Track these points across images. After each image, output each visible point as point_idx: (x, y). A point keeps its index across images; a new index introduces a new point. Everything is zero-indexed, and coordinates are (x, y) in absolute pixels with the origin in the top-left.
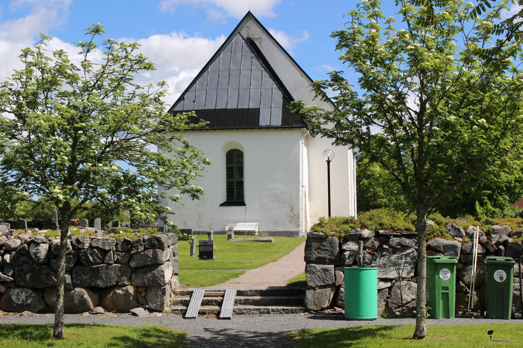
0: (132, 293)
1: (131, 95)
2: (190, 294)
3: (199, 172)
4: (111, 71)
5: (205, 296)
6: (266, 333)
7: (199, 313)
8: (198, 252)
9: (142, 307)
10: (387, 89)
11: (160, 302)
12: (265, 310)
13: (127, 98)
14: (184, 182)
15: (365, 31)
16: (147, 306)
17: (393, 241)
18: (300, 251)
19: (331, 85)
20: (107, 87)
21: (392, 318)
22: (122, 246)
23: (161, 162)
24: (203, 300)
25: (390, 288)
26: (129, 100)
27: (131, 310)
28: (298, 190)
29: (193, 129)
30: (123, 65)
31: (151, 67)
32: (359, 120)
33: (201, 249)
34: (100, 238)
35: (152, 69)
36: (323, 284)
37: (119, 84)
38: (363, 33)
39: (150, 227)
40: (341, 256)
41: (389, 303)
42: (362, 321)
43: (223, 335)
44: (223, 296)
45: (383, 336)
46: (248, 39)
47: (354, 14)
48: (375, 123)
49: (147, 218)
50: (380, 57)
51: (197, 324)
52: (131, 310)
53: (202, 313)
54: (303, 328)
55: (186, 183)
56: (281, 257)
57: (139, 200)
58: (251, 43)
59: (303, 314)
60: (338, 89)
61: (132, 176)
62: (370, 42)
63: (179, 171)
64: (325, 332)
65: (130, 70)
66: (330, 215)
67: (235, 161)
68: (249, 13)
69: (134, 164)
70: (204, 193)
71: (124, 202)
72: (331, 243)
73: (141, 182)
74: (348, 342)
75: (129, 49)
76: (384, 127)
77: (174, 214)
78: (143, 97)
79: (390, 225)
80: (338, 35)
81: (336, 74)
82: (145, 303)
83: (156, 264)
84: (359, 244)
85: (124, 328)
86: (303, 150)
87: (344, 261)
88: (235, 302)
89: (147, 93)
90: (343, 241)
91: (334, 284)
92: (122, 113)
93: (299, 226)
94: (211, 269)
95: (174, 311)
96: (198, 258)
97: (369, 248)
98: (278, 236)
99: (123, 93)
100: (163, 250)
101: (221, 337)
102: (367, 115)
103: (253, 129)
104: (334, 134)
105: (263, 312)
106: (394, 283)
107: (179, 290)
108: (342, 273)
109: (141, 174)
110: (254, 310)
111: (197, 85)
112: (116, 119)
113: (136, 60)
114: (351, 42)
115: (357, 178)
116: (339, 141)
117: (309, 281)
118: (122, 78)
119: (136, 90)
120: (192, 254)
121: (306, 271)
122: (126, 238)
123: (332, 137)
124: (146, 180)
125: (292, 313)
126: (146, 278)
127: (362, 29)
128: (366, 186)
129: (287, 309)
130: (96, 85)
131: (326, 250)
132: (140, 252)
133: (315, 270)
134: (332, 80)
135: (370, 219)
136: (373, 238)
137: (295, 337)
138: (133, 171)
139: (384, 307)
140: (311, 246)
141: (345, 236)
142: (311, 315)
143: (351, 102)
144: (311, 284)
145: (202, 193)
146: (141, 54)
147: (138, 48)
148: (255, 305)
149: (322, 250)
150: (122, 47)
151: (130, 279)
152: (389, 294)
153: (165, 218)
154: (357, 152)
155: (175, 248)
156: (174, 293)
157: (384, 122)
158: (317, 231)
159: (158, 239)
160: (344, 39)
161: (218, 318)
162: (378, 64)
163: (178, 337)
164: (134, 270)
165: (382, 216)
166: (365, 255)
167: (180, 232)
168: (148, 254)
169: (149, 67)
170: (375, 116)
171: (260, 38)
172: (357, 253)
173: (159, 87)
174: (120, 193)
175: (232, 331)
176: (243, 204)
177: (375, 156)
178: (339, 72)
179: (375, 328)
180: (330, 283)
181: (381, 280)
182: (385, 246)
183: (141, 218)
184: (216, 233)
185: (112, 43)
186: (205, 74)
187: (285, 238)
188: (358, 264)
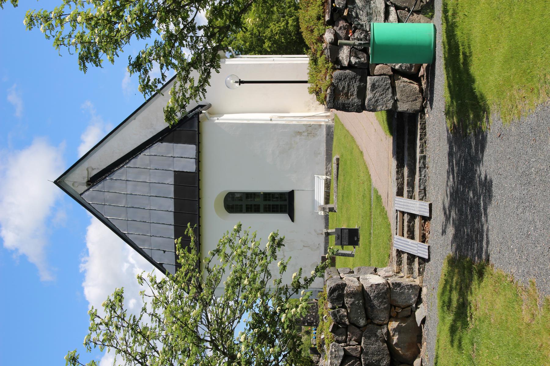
0: (397, 323)
1: (154, 319)
2: (400, 253)
3: (250, 237)
4: (125, 343)
5: (403, 235)
6: (449, 159)
7: (424, 242)
8: (349, 246)
9: (415, 312)
10: (151, 5)
11: (409, 289)
12: (422, 162)
13: (158, 323)
14: (262, 256)
15: (80, 29)
16: (414, 305)
17: (339, 3)
18: (349, 118)
19: (146, 71)
20: (144, 347)
21: (433, 6)
22: (339, 335)
23: (236, 283)
24: (407, 237)
25: (397, 8)
26: (160, 321)
27: (419, 325)
28: (276, 125)
29: (199, 244)
30: (117, 327)
31: (120, 293)
32: (189, 39)
33: (345, 243)
34: (329, 361)
35: (122, 293)
36: (390, 90)
37: (140, 333)
38: (81, 31)
39: (317, 303)
40: (356, 67)
41: (415, 9)
42: (437, 42)
43: (450, 212)
44: (403, 213)
45: (454, 14)
46: (89, 184)
47: (60, 42)
48: (193, 19)
49: (306, 300)
50: (112, 11)
51: (436, 243)
52: (419, 325)
53: (423, 239)
54: (443, 114)
55: (264, 253)
56: (358, 147)
57: (283, 311)
58: (93, 181)
59: (427, 115)
60: (151, 63)
61: (253, 318)
62: (93, 23)
63: (248, 262)
64: (449, 86)
65: (123, 319)
66: (306, 82)
68: (56, 182)
69: (237, 315)
70: (276, 232)
71: (285, 327)
72: (340, 80)
73: (262, 308)
74: (461, 56)
75: (98, 321)
76: (198, 9)
77: (301, 269)
78: (156, 302)
79: (319, 6)
80: (84, 63)
81: (132, 65)
82: (410, 308)
83: (362, 293)
84: (342, 45)
85: (440, 332)
86: (227, 118)
87: (362, 63)
88: (411, 198)
89: (151, 298)
90: (338, 65)
91: (390, 76)
92: (176, 328)
93: (321, 125)
94: (370, 230)
95: (420, 273)
96: (357, 247)
97: (347, 33)
98: (332, 150)
99: (151, 329)
100: (345, 285)
101: (453, 214)
102: (183, 29)
103: (199, 180)
104: (205, 70)
105: (424, 164)
106: (391, 3)
107: (395, 267)
108: (377, 67)
109: (251, 307)
110: (421, 175)
111: (145, 247)
112: (183, 335)
113: (111, 311)
114: (93, 46)
115: (261, 54)
116: (217, 67)
117: (387, 107)
118: (132, 329)
119: (148, 312)
120: (352, 255)
121: (374, 110)
122: (330, 330)
123: (209, 73)
124: (259, 302)
125: (425, 129)
126: (379, 306)
127: (77, 33)
128: (272, 44)
129: (421, 135)
130: (140, 360)
131: (349, 85)
132: (347, 313)
133: (373, 100)
134: (140, 71)
135: (312, 31)
136: (335, 28)
137: (454, 123)
138: (247, 317)
139: (421, 16)
140: (344, 105)
141: (332, 62)
142: (428, 106)
143: (168, 48)
144: (390, 105)
145: (277, 235)
146: (104, 305)
147: (96, 310)
148: (414, 173)
149: (348, 90)
150: (94, 329)
151: (381, 326)
152: (403, 9)
153: (306, 280)
154: (231, 54)
155: (343, 271)
156: (398, 273)
157: (192, 8)
158: (326, 97)
159: (332, 291)
160: (89, 56)
161: (429, 218)
162: (121, 14)
163: (451, 266)
164: (369, 321)
165: (308, 17)
166: (356, 38)
167: (324, 263)
168: (350, 303)
169: (119, 296)
170: (184, 19)
171: (87, 169)
172: (353, 47)
173: (145, 284)
174: (274, 333)
175: (446, 200)
176: (291, 194)
177: (234, 20)
178: (130, 61)
179: (445, 24)
180: (390, 82)
181: (386, 18)
182: (345, 14)
183: (306, 308)
184: (327, 226)
185: (89, 340)
186: (130, 237)
187: (335, 143)
188: (366, 46)
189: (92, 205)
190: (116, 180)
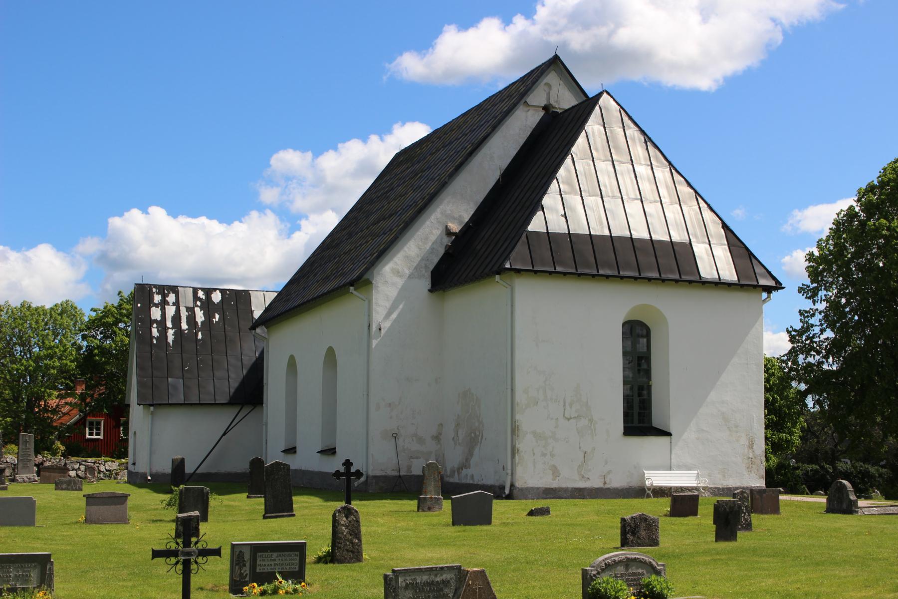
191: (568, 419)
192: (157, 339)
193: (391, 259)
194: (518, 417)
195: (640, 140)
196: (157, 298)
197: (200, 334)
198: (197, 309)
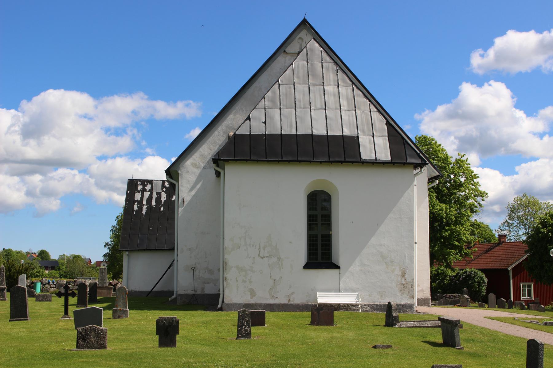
67: (320, 210)
189: (305, 50)
190: (337, 75)
191: (262, 258)
192: (136, 211)
193: (191, 156)
194: (226, 256)
195: (333, 69)
196: (140, 188)
197: (162, 208)
198: (163, 193)
